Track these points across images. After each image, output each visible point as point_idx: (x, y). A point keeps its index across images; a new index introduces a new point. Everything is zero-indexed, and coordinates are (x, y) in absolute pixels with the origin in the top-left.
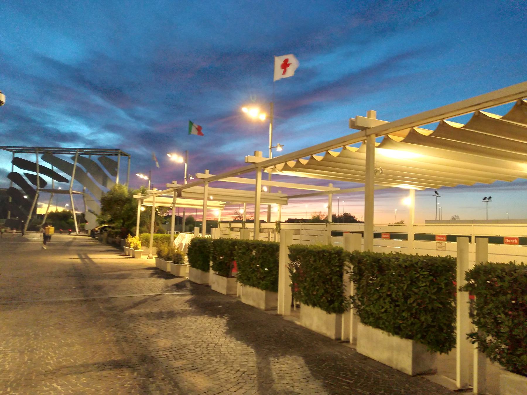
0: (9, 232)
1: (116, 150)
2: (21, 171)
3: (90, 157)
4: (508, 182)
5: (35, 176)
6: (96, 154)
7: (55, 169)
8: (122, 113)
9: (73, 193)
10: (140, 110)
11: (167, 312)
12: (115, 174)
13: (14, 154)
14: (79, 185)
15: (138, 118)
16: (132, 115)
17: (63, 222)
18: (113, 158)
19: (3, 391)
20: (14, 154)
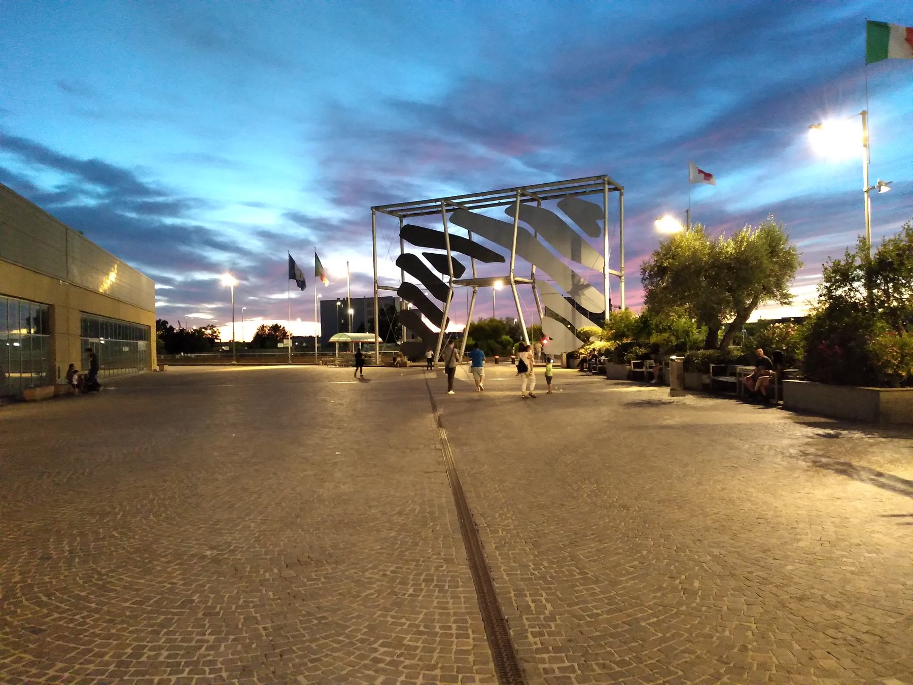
0: (410, 366)
1: (599, 177)
2: (418, 252)
3: (539, 204)
4: (727, 393)
5: (445, 257)
6: (552, 197)
7: (476, 238)
8: (516, 164)
9: (517, 282)
10: (545, 153)
11: (850, 476)
12: (596, 232)
13: (401, 221)
14: (525, 264)
15: (544, 167)
16: (529, 164)
17: (491, 342)
18: (592, 199)
19: (640, 622)
20: (401, 221)
